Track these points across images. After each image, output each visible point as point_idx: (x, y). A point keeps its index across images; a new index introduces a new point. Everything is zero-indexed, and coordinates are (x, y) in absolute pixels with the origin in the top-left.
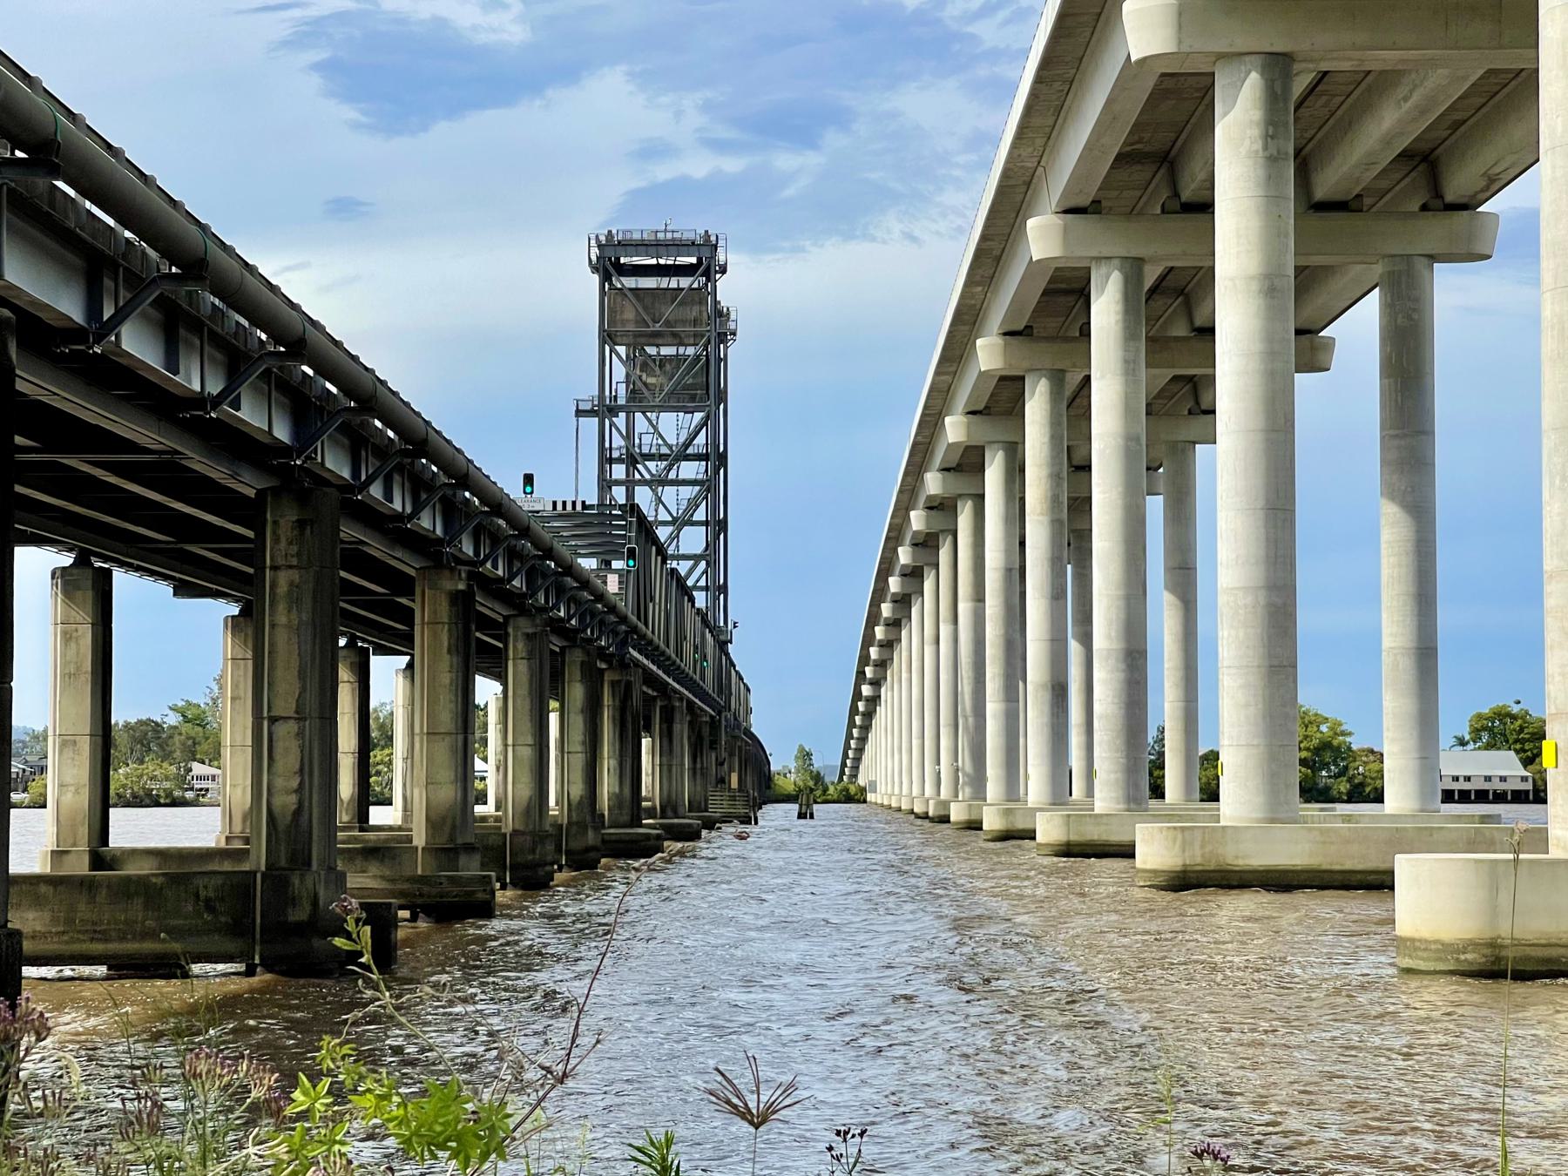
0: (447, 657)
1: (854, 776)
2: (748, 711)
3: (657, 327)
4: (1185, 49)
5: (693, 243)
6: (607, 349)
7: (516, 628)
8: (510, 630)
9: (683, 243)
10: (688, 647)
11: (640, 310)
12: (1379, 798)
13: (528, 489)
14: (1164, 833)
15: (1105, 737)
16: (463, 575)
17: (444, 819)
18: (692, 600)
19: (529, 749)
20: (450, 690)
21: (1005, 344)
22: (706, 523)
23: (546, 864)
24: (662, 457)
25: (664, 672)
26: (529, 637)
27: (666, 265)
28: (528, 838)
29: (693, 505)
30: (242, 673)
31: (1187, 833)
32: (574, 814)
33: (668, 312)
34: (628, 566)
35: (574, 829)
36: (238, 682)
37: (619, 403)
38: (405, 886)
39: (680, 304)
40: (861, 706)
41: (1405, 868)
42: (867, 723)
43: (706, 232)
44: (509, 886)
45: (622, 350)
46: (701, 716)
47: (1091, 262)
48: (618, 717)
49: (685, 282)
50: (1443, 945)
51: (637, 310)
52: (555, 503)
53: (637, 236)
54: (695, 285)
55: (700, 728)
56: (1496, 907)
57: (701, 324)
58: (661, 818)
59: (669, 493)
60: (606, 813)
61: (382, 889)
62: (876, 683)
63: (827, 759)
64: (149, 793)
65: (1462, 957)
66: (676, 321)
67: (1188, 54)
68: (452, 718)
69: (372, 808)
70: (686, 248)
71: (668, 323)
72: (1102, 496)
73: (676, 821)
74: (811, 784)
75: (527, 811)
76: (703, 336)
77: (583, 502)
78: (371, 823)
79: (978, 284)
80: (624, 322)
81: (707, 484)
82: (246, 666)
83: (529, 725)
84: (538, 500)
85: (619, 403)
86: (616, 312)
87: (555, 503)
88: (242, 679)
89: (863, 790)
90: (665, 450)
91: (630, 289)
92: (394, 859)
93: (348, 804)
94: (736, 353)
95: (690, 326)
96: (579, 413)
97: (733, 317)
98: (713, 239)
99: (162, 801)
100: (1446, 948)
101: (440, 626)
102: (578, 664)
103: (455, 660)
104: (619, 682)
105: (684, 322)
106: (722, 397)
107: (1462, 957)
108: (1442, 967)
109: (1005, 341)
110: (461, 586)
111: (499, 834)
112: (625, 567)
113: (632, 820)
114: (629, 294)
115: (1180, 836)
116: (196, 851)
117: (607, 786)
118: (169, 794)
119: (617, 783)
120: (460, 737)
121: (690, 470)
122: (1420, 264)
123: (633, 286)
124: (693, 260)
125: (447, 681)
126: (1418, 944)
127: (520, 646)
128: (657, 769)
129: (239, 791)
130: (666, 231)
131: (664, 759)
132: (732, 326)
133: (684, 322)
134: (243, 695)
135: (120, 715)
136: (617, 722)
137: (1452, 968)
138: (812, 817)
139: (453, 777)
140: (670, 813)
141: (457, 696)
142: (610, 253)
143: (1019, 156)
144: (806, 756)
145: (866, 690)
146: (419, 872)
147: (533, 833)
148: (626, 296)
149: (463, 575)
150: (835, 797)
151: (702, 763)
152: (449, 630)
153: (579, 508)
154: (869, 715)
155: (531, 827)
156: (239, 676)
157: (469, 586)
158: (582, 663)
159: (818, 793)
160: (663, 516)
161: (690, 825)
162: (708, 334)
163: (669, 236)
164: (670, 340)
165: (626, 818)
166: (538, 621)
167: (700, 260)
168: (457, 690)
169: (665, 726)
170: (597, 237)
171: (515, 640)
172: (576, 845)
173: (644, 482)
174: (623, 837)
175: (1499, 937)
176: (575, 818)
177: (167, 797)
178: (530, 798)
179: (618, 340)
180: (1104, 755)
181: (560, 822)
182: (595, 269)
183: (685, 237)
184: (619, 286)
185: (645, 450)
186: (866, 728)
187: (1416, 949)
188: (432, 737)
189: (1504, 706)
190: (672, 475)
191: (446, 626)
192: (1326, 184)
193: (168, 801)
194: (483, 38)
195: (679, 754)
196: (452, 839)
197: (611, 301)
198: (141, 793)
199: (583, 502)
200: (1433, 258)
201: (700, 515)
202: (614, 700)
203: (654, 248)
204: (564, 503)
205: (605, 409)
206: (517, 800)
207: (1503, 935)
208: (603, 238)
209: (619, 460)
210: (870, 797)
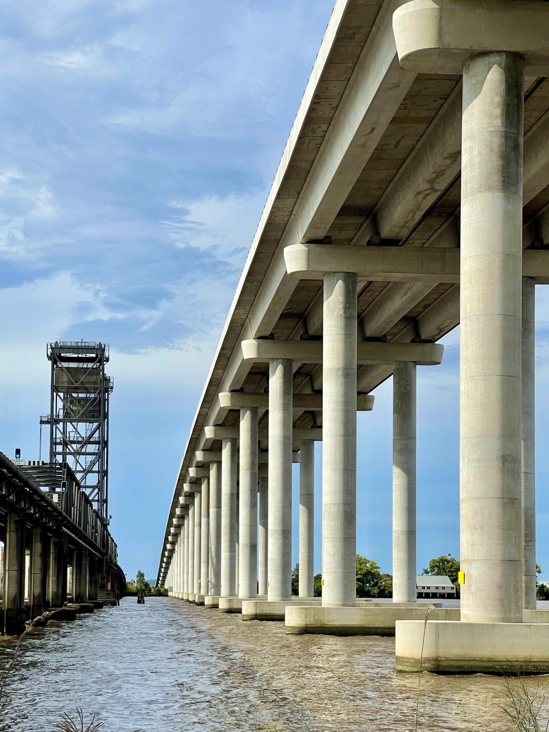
1: (163, 584)
2: (116, 555)
4: (311, 269)
5: (94, 348)
6: (55, 394)
8: (8, 519)
10: (89, 527)
12: (390, 596)
13: (18, 456)
14: (298, 610)
18: (91, 506)
19: (15, 572)
22: (98, 472)
24: (79, 442)
26: (16, 522)
29: (93, 464)
31: (308, 610)
32: (36, 601)
33: (82, 378)
34: (62, 490)
35: (36, 608)
37: (60, 418)
39: (88, 374)
40: (166, 553)
41: (400, 626)
49: (90, 365)
51: (68, 377)
52: (30, 462)
54: (95, 367)
56: (438, 643)
57: (97, 384)
59: (82, 458)
60: (51, 601)
62: (173, 543)
63: (151, 577)
65: (423, 665)
66: (86, 382)
71: (82, 383)
74: (144, 587)
75: (14, 600)
76: (98, 389)
77: (43, 462)
79: (220, 369)
81: (99, 454)
84: (22, 461)
85: (60, 418)
86: (59, 378)
87: (30, 462)
89: (166, 591)
90: (80, 439)
91: (66, 368)
94: (112, 397)
95: (92, 385)
96: (42, 422)
97: (111, 381)
98: (103, 346)
102: (39, 534)
105: (89, 383)
106: (106, 416)
107: (423, 665)
108: (415, 669)
114: (65, 370)
115: (304, 612)
117: (51, 588)
121: (91, 448)
122: (411, 365)
123: (67, 366)
124: (94, 355)
126: (405, 660)
127: (12, 526)
128: (74, 581)
130: (82, 342)
131: (78, 576)
132: (111, 385)
133: (89, 383)
138: (144, 603)
142: (57, 351)
144: (141, 575)
145: (169, 546)
148: (63, 370)
150: (154, 594)
153: (41, 464)
154: (170, 558)
159: (147, 592)
160: (79, 468)
162: (100, 388)
163: (83, 344)
164: (83, 390)
167: (97, 355)
173: (70, 453)
176: (36, 603)
178: (16, 594)
180: (272, 576)
182: (49, 358)
184: (60, 366)
185: (71, 439)
186: (168, 563)
187: (404, 662)
190: (83, 450)
192: (371, 329)
197: (56, 373)
199: (43, 462)
200: (416, 363)
201: (96, 468)
202: (55, 550)
207: (441, 655)
208: (53, 345)
209: (60, 444)
210: (170, 594)
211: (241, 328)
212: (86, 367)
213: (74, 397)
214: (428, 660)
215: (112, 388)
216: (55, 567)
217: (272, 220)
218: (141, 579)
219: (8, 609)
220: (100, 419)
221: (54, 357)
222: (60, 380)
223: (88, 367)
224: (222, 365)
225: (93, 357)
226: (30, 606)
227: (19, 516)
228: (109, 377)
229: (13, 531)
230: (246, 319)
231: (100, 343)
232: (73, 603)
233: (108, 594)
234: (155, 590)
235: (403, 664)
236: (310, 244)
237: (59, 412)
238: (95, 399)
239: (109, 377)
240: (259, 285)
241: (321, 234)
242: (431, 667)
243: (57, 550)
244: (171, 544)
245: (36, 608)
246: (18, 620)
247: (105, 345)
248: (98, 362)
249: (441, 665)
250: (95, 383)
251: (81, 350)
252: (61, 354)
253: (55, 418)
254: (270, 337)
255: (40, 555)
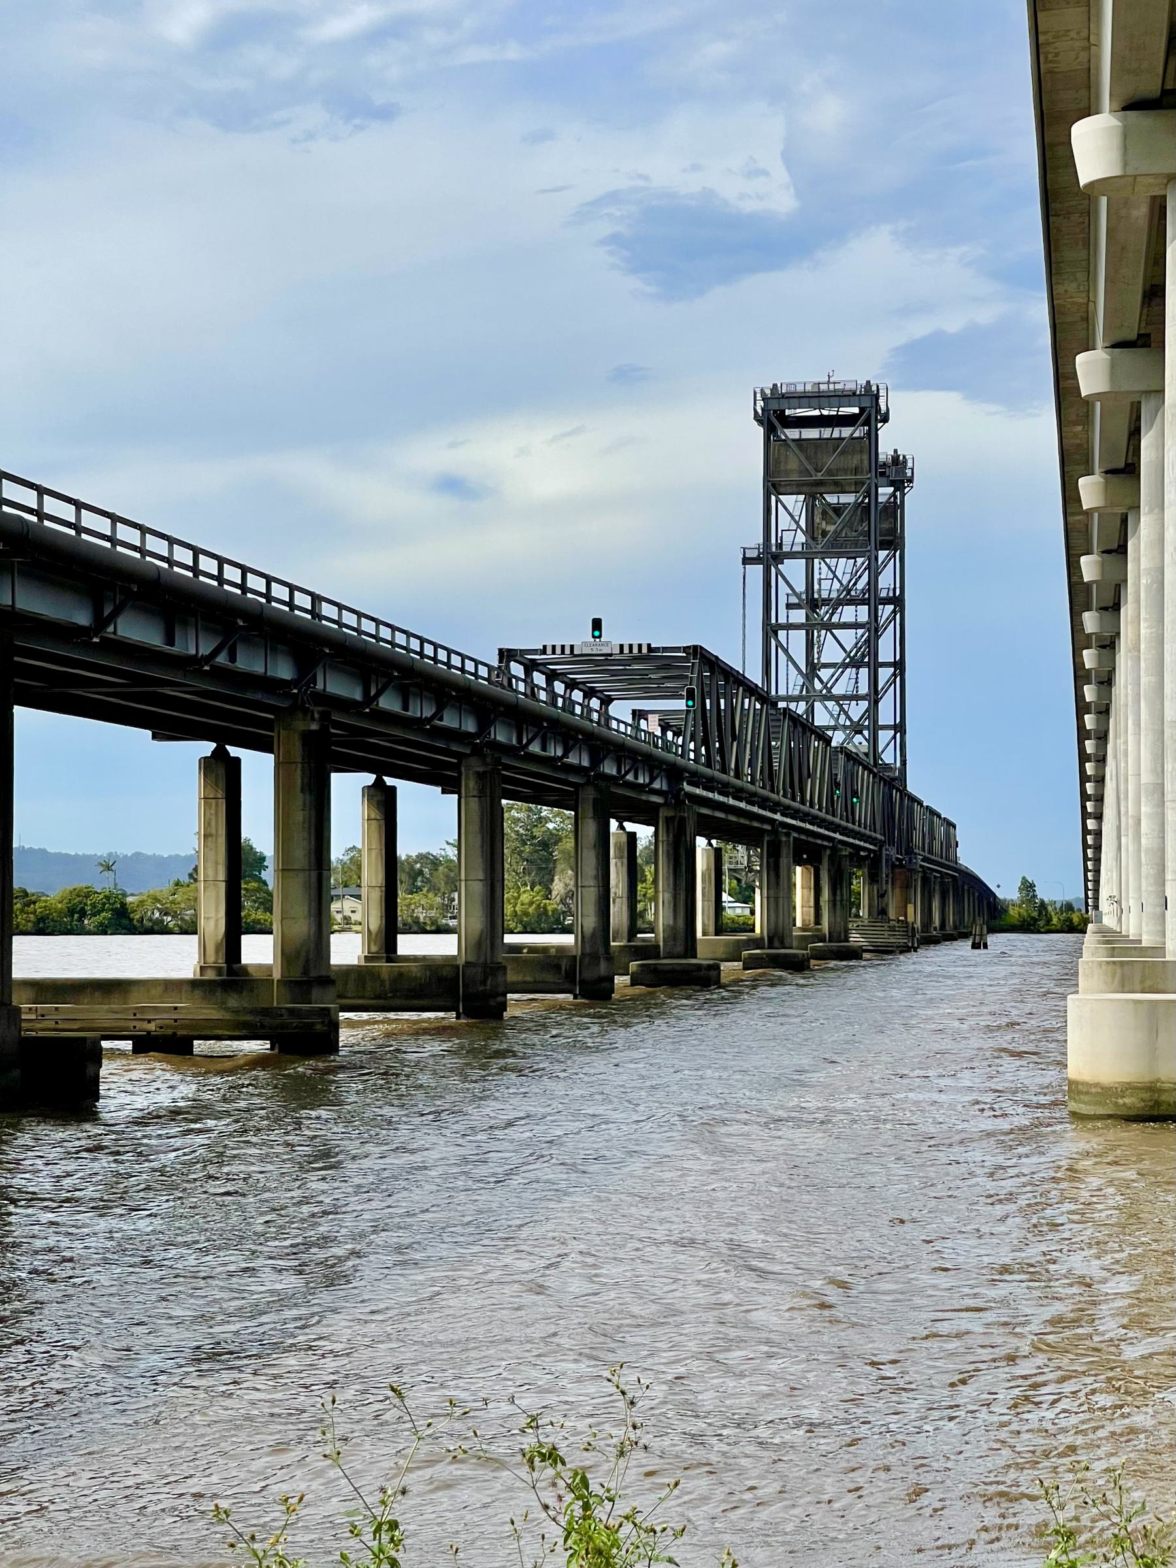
0: (300, 796)
3: (819, 476)
4: (1130, 171)
5: (854, 394)
6: (773, 498)
7: (468, 768)
8: (463, 769)
9: (845, 393)
11: (803, 460)
13: (597, 633)
14: (1104, 967)
15: (1151, 871)
16: (316, 716)
17: (298, 953)
19: (480, 884)
20: (304, 828)
21: (1106, 482)
23: (498, 995)
25: (760, 807)
26: (480, 776)
27: (829, 416)
28: (480, 969)
30: (213, 812)
31: (1126, 968)
32: (587, 946)
33: (830, 461)
34: (687, 706)
35: (587, 960)
36: (210, 820)
37: (784, 550)
38: (249, 1018)
39: (842, 453)
42: (1097, 857)
43: (868, 382)
44: (462, 1015)
45: (794, 502)
46: (841, 850)
47: (1141, 396)
48: (671, 852)
49: (846, 432)
50: (1102, 1089)
51: (800, 461)
52: (622, 646)
53: (800, 388)
54: (856, 435)
55: (840, 863)
56: (1156, 1049)
57: (862, 472)
58: (768, 948)
60: (661, 944)
61: (229, 1020)
64: (416, 921)
65: (1120, 1101)
66: (838, 470)
67: (1135, 177)
68: (305, 855)
69: (244, 938)
70: (847, 398)
71: (830, 472)
72: (1149, 631)
73: (782, 951)
74: (1035, 914)
75: (479, 944)
76: (863, 484)
77: (649, 645)
78: (399, 953)
80: (787, 473)
81: (867, 626)
82: (217, 805)
83: (480, 860)
85: (784, 550)
86: (780, 462)
87: (622, 646)
88: (213, 817)
91: (794, 440)
92: (252, 991)
93: (377, 935)
94: (912, 500)
95: (851, 474)
96: (746, 561)
97: (910, 465)
98: (874, 388)
99: (428, 928)
100: (1105, 1092)
101: (293, 766)
102: (591, 802)
103: (308, 797)
104: (672, 818)
105: (845, 471)
107: (1120, 1101)
108: (1101, 1111)
109: (1105, 479)
110: (314, 727)
111: (453, 966)
112: (685, 708)
113: (686, 949)
114: (791, 444)
115: (1119, 971)
116: (69, 983)
118: (434, 922)
119: (672, 918)
120: (314, 874)
123: (797, 437)
124: (856, 410)
125: (301, 819)
126: (1080, 1087)
127: (472, 784)
128: (765, 901)
129: (212, 923)
130: (829, 382)
131: (772, 892)
133: (845, 471)
134: (214, 832)
135: (406, 849)
136: (672, 858)
137: (1110, 1113)
138: (986, 947)
139: (306, 913)
140: (776, 944)
141: (310, 833)
142: (774, 405)
143: (1066, 291)
144: (1028, 887)
145: (1091, 824)
146: (275, 1005)
147: (485, 965)
148: (789, 446)
149: (316, 716)
150: (1059, 927)
151: (842, 895)
152: (303, 771)
153: (645, 650)
155: (482, 960)
156: (211, 814)
157: (322, 726)
158: (594, 799)
159: (1041, 923)
161: (795, 955)
162: (868, 481)
163: (831, 387)
164: (832, 488)
165: (680, 949)
166: (489, 760)
167: (862, 410)
168: (309, 828)
169: (772, 860)
170: (762, 390)
171: (467, 778)
172: (589, 975)
174: (677, 968)
175: (1158, 1080)
176: (588, 950)
177: (432, 924)
178: (482, 931)
179: (782, 490)
180: (1150, 889)
181: (574, 954)
183: (848, 387)
184: (783, 437)
185: (825, 595)
187: (1079, 1093)
188: (285, 873)
189: (110, 854)
190: (835, 619)
191: (300, 765)
193: (433, 928)
194: (750, 206)
195: (786, 887)
196: (306, 971)
198: (410, 920)
199: (649, 645)
202: (668, 836)
203: (817, 399)
204: (631, 646)
205: (769, 556)
206: (469, 931)
207: (1163, 1079)
208: (768, 392)
211: (1085, 326)
212: (838, 436)
213: (829, 504)
214: (1129, 1088)
215: (911, 480)
216: (668, 872)
217: (1051, 62)
218: (1028, 895)
219: (466, 962)
220: (869, 548)
221: (769, 419)
222: (782, 468)
223: (843, 436)
224: (1078, 415)
225: (854, 415)
226: (575, 957)
227: (485, 764)
228: (904, 457)
229: (474, 796)
230: (1088, 304)
231: (868, 382)
232: (762, 948)
233: (892, 929)
234: (1059, 919)
235: (1077, 1098)
236: (1128, 112)
237: (782, 537)
238: (857, 505)
239: (904, 457)
240: (1087, 221)
241: (1151, 86)
242: (1139, 1105)
243: (671, 836)
244: (1095, 818)
245: (587, 960)
246: (488, 988)
247: (878, 387)
248: (863, 425)
249: (1164, 1102)
250: (856, 471)
251: (826, 399)
252: (784, 411)
253: (774, 549)
254: (1140, 342)
255: (595, 846)
